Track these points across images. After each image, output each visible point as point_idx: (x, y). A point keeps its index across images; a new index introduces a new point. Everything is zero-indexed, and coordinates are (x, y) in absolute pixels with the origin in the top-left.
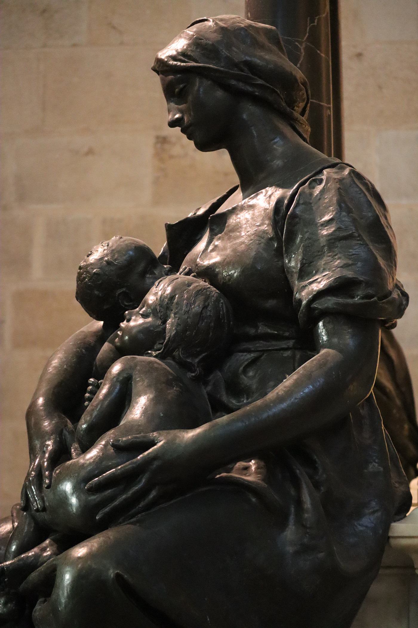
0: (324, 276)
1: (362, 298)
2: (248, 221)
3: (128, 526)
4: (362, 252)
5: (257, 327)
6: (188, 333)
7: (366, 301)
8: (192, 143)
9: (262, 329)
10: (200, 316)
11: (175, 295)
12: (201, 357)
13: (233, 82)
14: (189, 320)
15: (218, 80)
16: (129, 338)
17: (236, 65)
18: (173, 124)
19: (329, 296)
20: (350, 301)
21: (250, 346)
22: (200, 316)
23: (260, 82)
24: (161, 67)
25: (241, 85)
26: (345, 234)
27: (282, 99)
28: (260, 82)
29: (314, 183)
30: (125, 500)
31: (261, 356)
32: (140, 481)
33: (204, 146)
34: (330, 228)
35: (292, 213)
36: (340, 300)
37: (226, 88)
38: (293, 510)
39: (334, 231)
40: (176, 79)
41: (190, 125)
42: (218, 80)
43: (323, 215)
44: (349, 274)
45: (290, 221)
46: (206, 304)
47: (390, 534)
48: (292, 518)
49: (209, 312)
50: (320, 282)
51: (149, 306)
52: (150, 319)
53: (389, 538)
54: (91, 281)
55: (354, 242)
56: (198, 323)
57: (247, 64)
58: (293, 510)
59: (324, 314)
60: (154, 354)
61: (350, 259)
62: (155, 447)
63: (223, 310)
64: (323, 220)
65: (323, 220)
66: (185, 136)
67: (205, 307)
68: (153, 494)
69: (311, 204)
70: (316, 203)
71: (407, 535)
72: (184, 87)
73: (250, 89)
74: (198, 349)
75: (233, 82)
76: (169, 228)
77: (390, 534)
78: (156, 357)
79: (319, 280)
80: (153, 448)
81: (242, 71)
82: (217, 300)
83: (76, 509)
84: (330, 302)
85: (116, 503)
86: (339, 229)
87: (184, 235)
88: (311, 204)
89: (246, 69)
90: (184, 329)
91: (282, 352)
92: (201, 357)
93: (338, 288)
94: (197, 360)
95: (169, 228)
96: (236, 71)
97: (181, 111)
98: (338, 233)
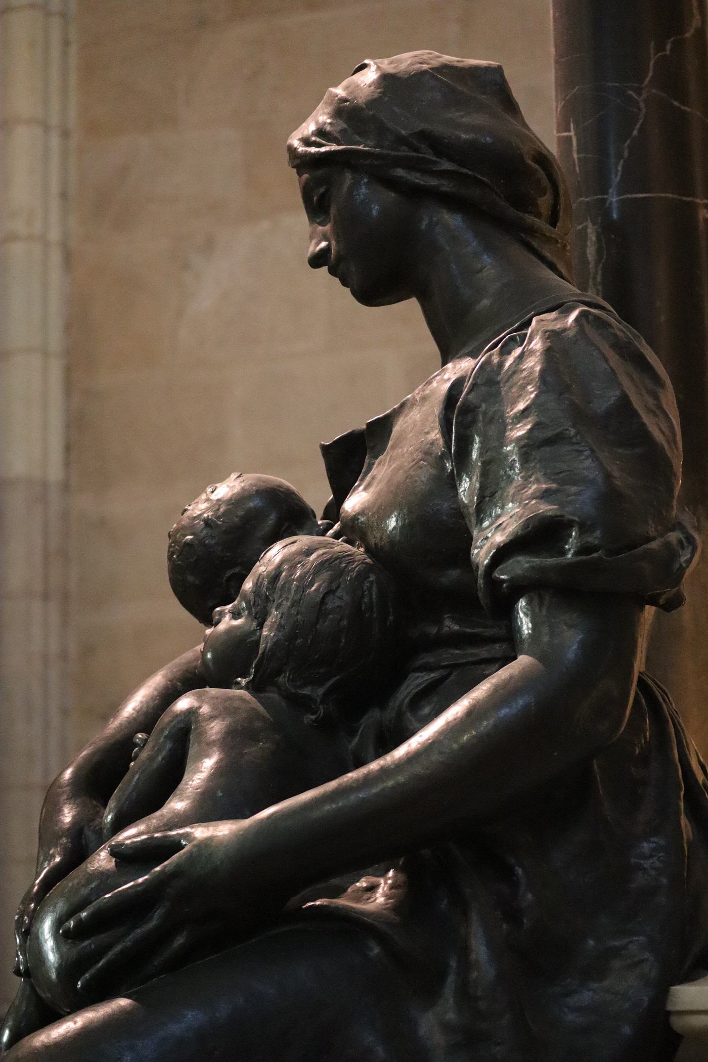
0: (511, 517)
1: (576, 554)
2: (415, 426)
3: (15, 995)
4: (586, 466)
5: (439, 622)
6: (299, 641)
7: (584, 558)
8: (347, 291)
9: (450, 625)
10: (320, 606)
11: (281, 573)
12: (328, 684)
13: (400, 172)
14: (299, 617)
15: (376, 170)
16: (213, 655)
17: (402, 141)
18: (317, 261)
19: (521, 555)
20: (559, 560)
21: (428, 659)
22: (320, 608)
23: (447, 165)
24: (302, 163)
25: (416, 178)
26: (549, 433)
27: (496, 193)
28: (447, 165)
29: (512, 344)
30: (122, 952)
31: (445, 678)
32: (151, 918)
33: (370, 295)
34: (525, 425)
35: (463, 404)
36: (536, 561)
37: (392, 184)
38: (453, 964)
39: (530, 430)
40: (320, 179)
41: (340, 258)
42: (376, 170)
43: (514, 403)
44: (545, 508)
45: (460, 419)
46: (334, 586)
47: (670, 1007)
48: (451, 979)
49: (342, 598)
50: (505, 529)
51: (245, 598)
52: (239, 622)
53: (669, 1013)
54: (181, 557)
55: (566, 448)
56: (317, 623)
57: (423, 136)
58: (453, 964)
59: (518, 589)
60: (244, 682)
61: (554, 481)
62: (182, 851)
63: (371, 595)
64: (515, 410)
65: (515, 410)
66: (337, 280)
67: (329, 592)
68: (179, 941)
69: (498, 383)
70: (507, 381)
71: (702, 1008)
72: (327, 191)
73: (433, 182)
74: (322, 671)
75: (400, 172)
76: (325, 450)
77: (670, 1007)
78: (247, 688)
79: (504, 525)
80: (177, 854)
81: (416, 150)
82: (362, 575)
83: (58, 974)
84: (521, 564)
85: (111, 954)
86: (537, 426)
87: (348, 458)
88: (498, 383)
89: (423, 147)
90: (292, 635)
91: (483, 666)
92: (328, 684)
93: (538, 536)
94: (321, 691)
95: (325, 450)
96: (404, 152)
97: (325, 237)
98: (536, 433)
